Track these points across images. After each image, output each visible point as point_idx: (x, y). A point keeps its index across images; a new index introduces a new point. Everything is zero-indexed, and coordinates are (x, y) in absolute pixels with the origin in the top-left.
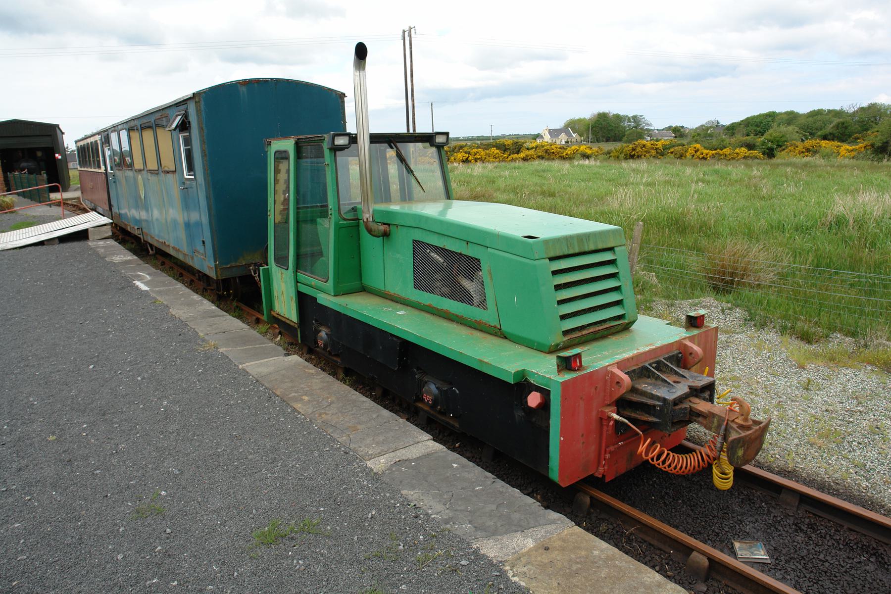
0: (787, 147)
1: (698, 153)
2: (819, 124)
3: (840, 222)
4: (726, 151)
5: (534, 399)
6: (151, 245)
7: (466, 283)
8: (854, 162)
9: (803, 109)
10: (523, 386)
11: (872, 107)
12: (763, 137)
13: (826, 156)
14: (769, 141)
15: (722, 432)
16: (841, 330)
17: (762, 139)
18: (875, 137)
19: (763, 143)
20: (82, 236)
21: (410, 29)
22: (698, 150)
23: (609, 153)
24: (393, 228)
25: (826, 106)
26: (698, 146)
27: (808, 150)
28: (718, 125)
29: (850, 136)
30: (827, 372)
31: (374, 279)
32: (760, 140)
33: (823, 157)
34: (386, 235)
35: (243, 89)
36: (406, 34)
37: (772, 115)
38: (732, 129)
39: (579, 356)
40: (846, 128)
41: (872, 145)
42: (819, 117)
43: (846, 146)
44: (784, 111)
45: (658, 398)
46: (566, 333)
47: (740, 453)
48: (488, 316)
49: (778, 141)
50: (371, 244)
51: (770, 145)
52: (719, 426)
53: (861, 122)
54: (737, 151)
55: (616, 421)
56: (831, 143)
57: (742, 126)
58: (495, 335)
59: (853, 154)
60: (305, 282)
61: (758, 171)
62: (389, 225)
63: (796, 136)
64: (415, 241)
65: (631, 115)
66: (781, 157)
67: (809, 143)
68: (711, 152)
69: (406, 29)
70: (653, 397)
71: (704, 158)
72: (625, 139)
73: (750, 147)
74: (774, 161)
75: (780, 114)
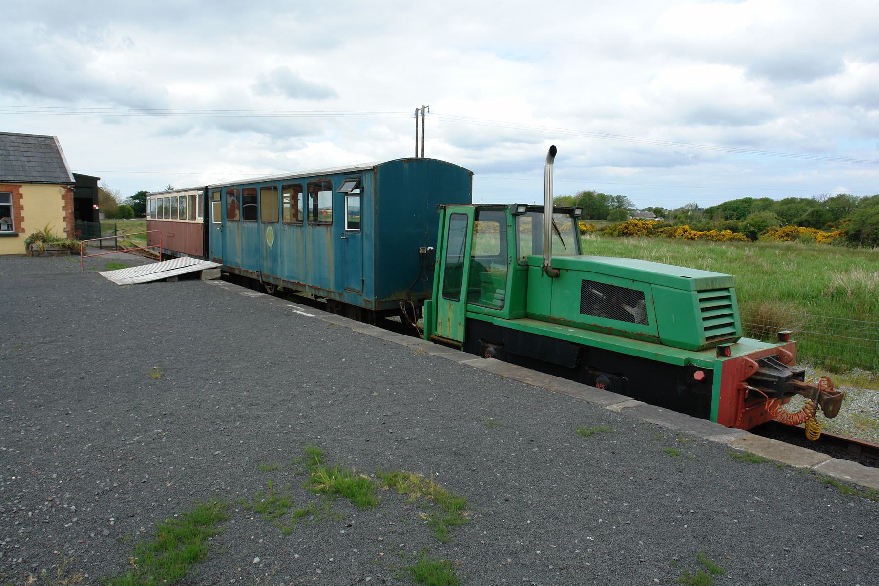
1: (687, 234)
2: (792, 212)
3: (840, 293)
4: (713, 232)
5: (699, 376)
6: (268, 284)
7: (629, 309)
8: (831, 247)
10: (690, 368)
11: (841, 197)
12: (742, 221)
13: (806, 241)
14: (751, 225)
15: (817, 397)
16: (859, 366)
17: (745, 223)
18: (848, 225)
19: (746, 227)
20: (195, 276)
21: (424, 108)
22: (686, 231)
23: (602, 230)
24: (563, 272)
25: (799, 195)
26: (686, 227)
27: (787, 235)
28: (696, 209)
29: (824, 224)
30: (856, 391)
31: (533, 309)
32: (741, 224)
33: (804, 242)
34: (557, 276)
35: (406, 165)
37: (748, 201)
39: (728, 347)
40: (820, 216)
41: (847, 233)
42: (793, 205)
43: (821, 234)
44: (759, 197)
45: (775, 377)
46: (707, 339)
47: (831, 408)
48: (649, 330)
49: (759, 226)
50: (540, 284)
51: (751, 228)
52: (814, 394)
53: (831, 211)
54: (723, 232)
55: (750, 390)
57: (720, 210)
58: (653, 342)
59: (829, 240)
60: (475, 310)
61: (749, 251)
62: (559, 269)
64: (583, 281)
65: (614, 195)
66: (763, 240)
67: (788, 228)
69: (420, 107)
70: (770, 376)
71: (692, 239)
72: (609, 217)
73: (734, 230)
74: (757, 242)
75: (756, 200)
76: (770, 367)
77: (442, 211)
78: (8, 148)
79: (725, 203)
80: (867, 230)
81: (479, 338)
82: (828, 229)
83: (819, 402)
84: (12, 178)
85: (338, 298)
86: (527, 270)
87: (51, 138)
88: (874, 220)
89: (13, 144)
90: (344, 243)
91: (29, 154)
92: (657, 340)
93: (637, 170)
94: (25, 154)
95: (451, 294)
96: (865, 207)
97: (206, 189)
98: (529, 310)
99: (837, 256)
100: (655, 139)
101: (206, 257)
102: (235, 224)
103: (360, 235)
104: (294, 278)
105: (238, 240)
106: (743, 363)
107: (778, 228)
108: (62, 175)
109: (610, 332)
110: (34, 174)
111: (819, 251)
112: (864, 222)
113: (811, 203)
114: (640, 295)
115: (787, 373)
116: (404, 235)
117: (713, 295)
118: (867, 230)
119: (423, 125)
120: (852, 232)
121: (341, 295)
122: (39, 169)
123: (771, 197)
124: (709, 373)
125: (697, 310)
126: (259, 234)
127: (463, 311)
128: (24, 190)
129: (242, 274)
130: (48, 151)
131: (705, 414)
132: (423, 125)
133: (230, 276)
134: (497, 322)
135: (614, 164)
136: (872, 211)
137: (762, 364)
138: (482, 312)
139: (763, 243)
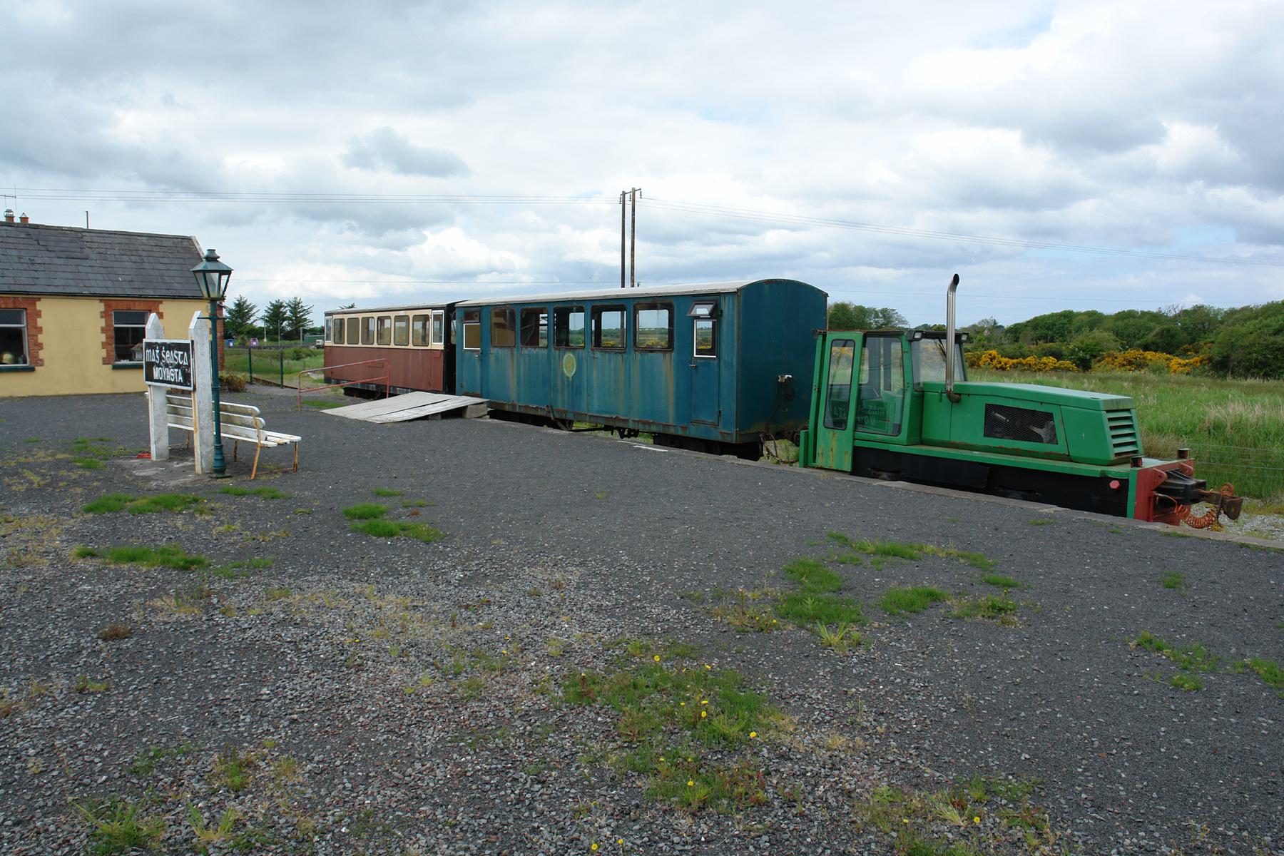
0: (1103, 358)
1: (995, 362)
2: (1131, 330)
3: (1216, 429)
4: (1030, 360)
5: (1114, 485)
7: (1036, 430)
9: (1109, 308)
10: (1105, 479)
11: (1198, 310)
13: (1157, 370)
14: (1080, 349)
20: (458, 413)
21: (634, 191)
24: (964, 398)
25: (1139, 307)
26: (994, 352)
27: (1130, 363)
28: (995, 327)
29: (1178, 347)
31: (930, 434)
33: (1154, 372)
35: (767, 287)
36: (627, 196)
37: (1068, 315)
38: (1016, 332)
41: (1210, 360)
42: (1131, 321)
48: (1060, 448)
51: (1081, 354)
53: (1184, 329)
54: (1044, 360)
56: (1158, 355)
63: (1113, 344)
65: (879, 308)
66: (1098, 370)
67: (1131, 353)
68: (1011, 361)
71: (1003, 369)
73: (1058, 356)
75: (1079, 314)
76: (1176, 478)
77: (820, 338)
79: (1036, 319)
80: (1237, 355)
81: (868, 462)
82: (1184, 354)
83: (1222, 507)
84: (150, 292)
85: (680, 433)
86: (923, 396)
87: (189, 239)
88: (1246, 342)
89: (146, 248)
90: (689, 374)
93: (902, 272)
95: (839, 424)
96: (1234, 324)
97: (450, 309)
99: (1204, 389)
100: (922, 227)
102: (507, 351)
105: (511, 369)
106: (1153, 473)
107: (1117, 353)
109: (1017, 452)
110: (176, 286)
111: (1178, 383)
112: (1232, 346)
113: (1156, 317)
114: (1049, 416)
115: (1192, 482)
116: (765, 361)
117: (1121, 417)
118: (1237, 355)
121: (684, 428)
123: (1099, 310)
124: (1124, 483)
125: (1107, 429)
126: (549, 363)
128: (43, 305)
129: (517, 410)
130: (187, 256)
131: (1123, 513)
133: (498, 413)
134: (893, 448)
135: (871, 263)
136: (1243, 330)
137: (1170, 476)
138: (874, 438)
139: (1099, 374)
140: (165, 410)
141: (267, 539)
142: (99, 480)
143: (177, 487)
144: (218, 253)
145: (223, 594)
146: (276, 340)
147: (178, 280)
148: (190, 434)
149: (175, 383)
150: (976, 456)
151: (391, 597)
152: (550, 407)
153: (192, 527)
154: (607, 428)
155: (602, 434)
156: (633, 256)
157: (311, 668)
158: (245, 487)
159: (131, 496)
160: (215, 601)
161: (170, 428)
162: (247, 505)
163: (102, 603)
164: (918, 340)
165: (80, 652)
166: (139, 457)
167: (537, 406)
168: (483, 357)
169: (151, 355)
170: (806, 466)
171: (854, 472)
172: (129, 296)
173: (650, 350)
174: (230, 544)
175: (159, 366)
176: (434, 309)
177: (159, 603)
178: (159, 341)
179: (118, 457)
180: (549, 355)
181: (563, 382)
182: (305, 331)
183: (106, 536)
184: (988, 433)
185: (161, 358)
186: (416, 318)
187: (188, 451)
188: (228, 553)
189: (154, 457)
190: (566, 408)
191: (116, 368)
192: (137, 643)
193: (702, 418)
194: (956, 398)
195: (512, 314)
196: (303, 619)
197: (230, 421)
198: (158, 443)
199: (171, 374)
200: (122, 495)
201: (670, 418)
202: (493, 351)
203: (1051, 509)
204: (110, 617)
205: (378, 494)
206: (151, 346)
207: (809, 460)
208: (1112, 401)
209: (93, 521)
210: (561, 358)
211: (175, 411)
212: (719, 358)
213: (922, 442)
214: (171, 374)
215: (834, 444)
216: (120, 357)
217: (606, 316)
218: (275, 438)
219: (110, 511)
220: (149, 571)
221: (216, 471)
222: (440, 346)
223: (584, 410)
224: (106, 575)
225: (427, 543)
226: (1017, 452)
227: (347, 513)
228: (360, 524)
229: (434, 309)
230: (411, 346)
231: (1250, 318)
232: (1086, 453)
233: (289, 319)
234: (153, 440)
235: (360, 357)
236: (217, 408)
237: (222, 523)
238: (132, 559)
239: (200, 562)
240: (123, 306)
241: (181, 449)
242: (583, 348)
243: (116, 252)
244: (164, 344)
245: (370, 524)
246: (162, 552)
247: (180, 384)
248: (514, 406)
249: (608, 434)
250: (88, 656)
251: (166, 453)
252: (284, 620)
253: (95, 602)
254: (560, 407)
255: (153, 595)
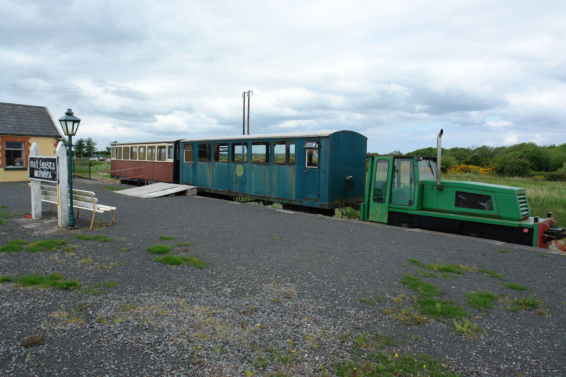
7: (482, 204)
11: (484, 147)
21: (249, 92)
25: (460, 146)
29: (480, 163)
31: (426, 205)
35: (342, 134)
36: (246, 94)
40: (478, 159)
41: (496, 169)
43: (482, 169)
46: (523, 216)
48: (495, 213)
49: (446, 164)
78: (19, 114)
79: (417, 151)
81: (396, 219)
82: (483, 166)
84: (24, 133)
85: (298, 204)
87: (44, 108)
88: (510, 161)
89: (22, 112)
90: (302, 176)
91: (32, 118)
92: (499, 217)
94: (30, 118)
98: (424, 206)
101: (176, 180)
103: (317, 170)
104: (260, 194)
105: (208, 172)
108: (54, 131)
109: (472, 214)
110: (38, 130)
113: (467, 150)
118: (507, 167)
119: (249, 102)
120: (499, 168)
122: (40, 127)
127: (387, 208)
129: (212, 192)
131: (531, 245)
132: (249, 102)
133: (201, 193)
134: (410, 212)
140: (40, 192)
141: (109, 267)
142: (5, 231)
143: (49, 234)
144: (73, 111)
145: (96, 307)
146: (80, 157)
147: (38, 127)
148: (56, 205)
149: (47, 179)
150: (452, 216)
151: (197, 307)
152: (230, 191)
153: (64, 260)
154: (256, 201)
155: (253, 203)
156: (248, 121)
157: (170, 366)
158: (88, 235)
159: (25, 241)
160: (91, 312)
161: (43, 202)
162: (92, 246)
163: (19, 317)
164: (421, 160)
165: (10, 358)
166: (25, 217)
167: (222, 190)
168: (194, 166)
169: (33, 164)
170: (364, 220)
171: (389, 223)
172: (13, 135)
173: (258, 163)
174: (88, 271)
175: (38, 170)
176: (168, 143)
177: (56, 315)
178: (38, 157)
179: (14, 217)
180: (229, 166)
181: (236, 178)
182: (94, 153)
183: (15, 267)
184: (457, 205)
185: (39, 166)
186: (149, 147)
187: (55, 214)
188: (89, 277)
189: (34, 217)
190: (238, 191)
191: (6, 169)
192: (48, 349)
193: (310, 197)
194: (441, 188)
195: (210, 145)
196: (150, 325)
197: (78, 199)
198: (36, 209)
199: (45, 174)
200: (20, 240)
201: (293, 197)
202: (200, 163)
203: (499, 243)
204: (26, 327)
205: (162, 239)
206: (33, 159)
207: (366, 217)
208: (519, 190)
209: (5, 257)
210: (235, 167)
211: (45, 193)
212: (319, 168)
213: (423, 209)
214: (45, 174)
215: (379, 210)
216: (8, 164)
217: (237, 147)
218: (103, 208)
219: (15, 251)
220: (44, 291)
221: (70, 226)
222: (172, 161)
223: (247, 192)
224: (19, 294)
225: (201, 269)
226: (472, 214)
227: (149, 251)
228: (161, 257)
229: (168, 143)
230: (146, 160)
231: (509, 152)
232: (500, 214)
233: (86, 147)
234: (33, 208)
235: (129, 167)
236: (71, 192)
237: (81, 258)
238: (33, 283)
239: (75, 285)
240: (10, 139)
241: (49, 212)
242: (247, 162)
243: (7, 113)
244: (41, 159)
245: (163, 257)
246: (52, 278)
247: (50, 179)
248: (210, 190)
249: (257, 203)
250: (16, 362)
251: (40, 215)
252: (138, 326)
253: (15, 315)
254: (234, 191)
255: (50, 309)
